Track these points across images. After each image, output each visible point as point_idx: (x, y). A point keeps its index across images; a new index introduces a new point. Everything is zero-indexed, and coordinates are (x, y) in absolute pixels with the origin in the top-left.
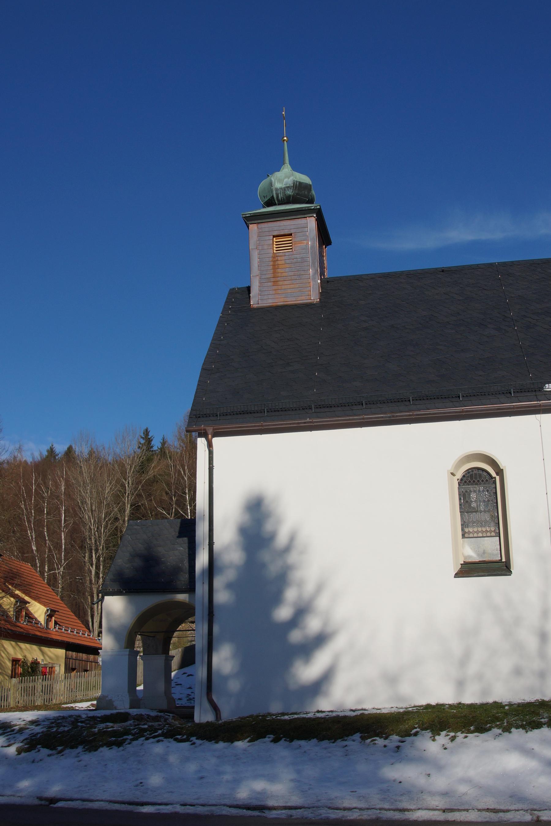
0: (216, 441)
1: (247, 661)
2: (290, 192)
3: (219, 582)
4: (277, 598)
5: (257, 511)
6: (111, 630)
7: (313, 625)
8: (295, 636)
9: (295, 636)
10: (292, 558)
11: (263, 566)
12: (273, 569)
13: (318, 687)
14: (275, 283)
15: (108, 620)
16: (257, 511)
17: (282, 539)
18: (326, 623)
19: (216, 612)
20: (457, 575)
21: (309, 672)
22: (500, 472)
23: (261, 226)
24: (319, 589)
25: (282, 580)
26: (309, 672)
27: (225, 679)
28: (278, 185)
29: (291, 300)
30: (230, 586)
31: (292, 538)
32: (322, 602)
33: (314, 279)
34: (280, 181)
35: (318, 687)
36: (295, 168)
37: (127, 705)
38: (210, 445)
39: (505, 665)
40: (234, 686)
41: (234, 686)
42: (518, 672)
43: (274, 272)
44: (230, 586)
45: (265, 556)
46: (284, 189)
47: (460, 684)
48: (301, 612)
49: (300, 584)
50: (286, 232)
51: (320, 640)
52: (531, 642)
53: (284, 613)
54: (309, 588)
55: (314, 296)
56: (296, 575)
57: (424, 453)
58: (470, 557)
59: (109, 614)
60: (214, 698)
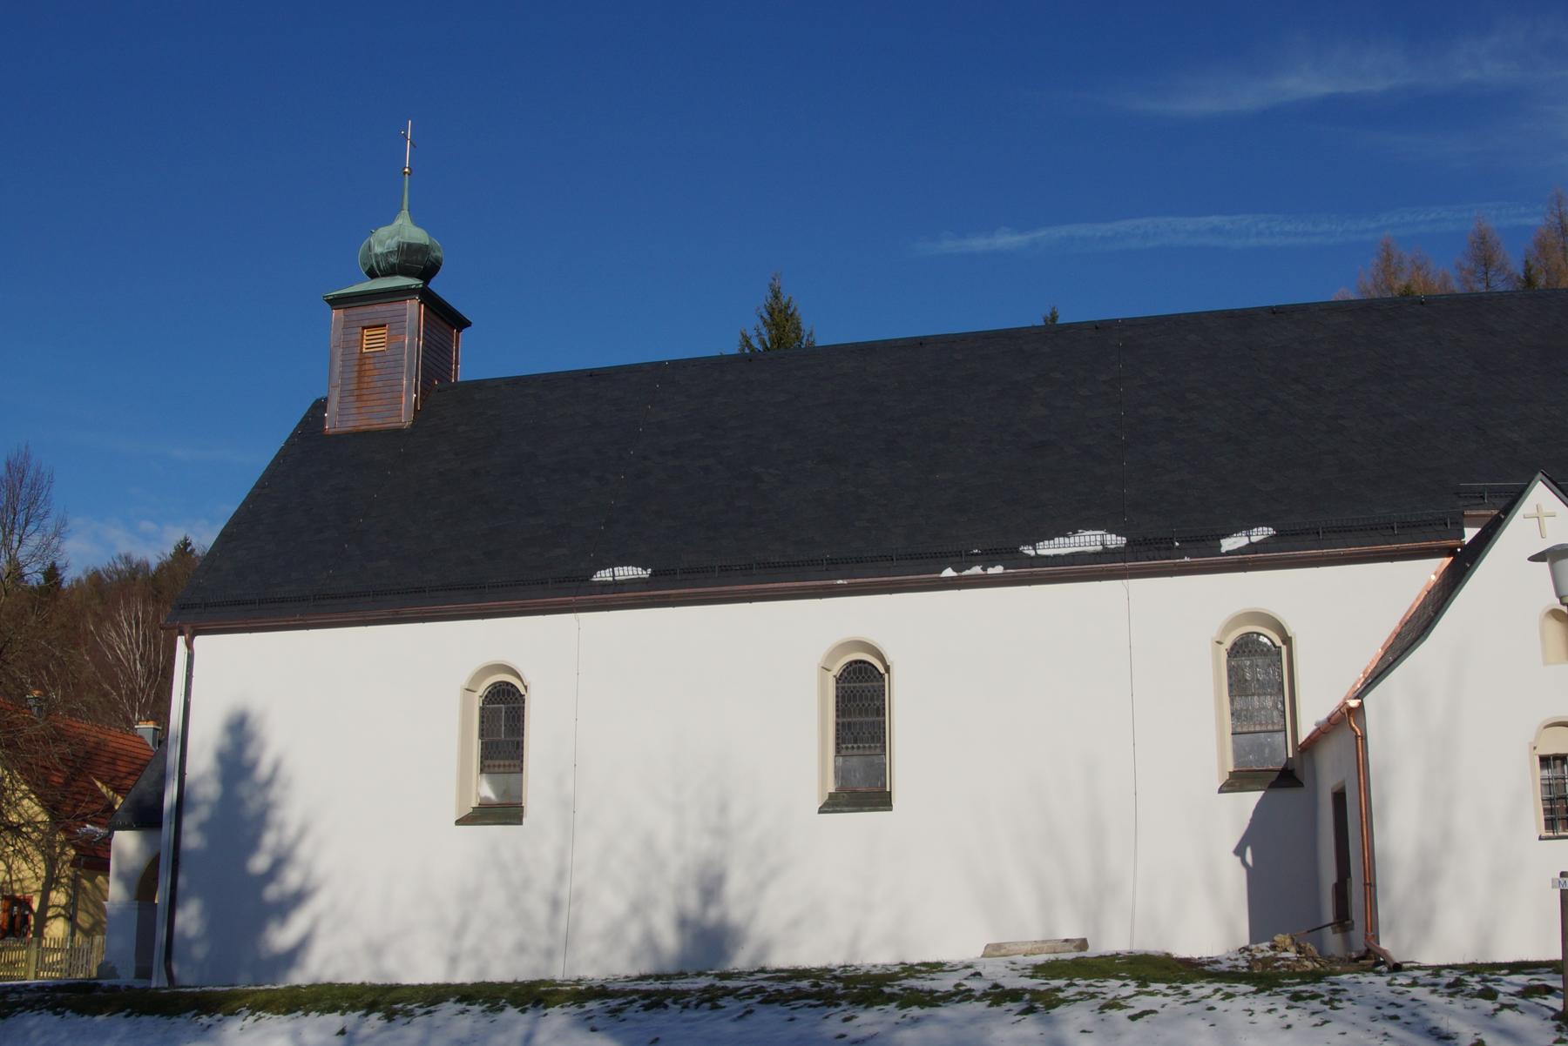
0: (200, 641)
1: (214, 920)
2: (393, 260)
3: (189, 822)
4: (253, 845)
5: (240, 730)
6: (121, 876)
7: (292, 878)
8: (272, 892)
9: (272, 892)
10: (275, 793)
12: (253, 806)
13: (292, 957)
14: (359, 398)
15: (118, 862)
16: (240, 730)
17: (264, 769)
20: (1221, 791)
21: (283, 937)
22: (887, 669)
23: (350, 311)
24: (302, 833)
26: (283, 937)
27: (189, 943)
28: (378, 250)
29: (376, 423)
30: (203, 827)
31: (276, 768)
32: (304, 851)
33: (408, 391)
34: (381, 243)
36: (417, 221)
37: (132, 974)
38: (189, 645)
39: (507, 938)
40: (199, 952)
41: (199, 952)
42: (521, 948)
43: (359, 382)
44: (203, 827)
45: (244, 790)
47: (453, 960)
48: (280, 862)
49: (281, 827)
50: (380, 322)
51: (298, 898)
52: (541, 911)
54: (291, 831)
55: (405, 418)
56: (277, 815)
57: (438, 659)
58: (487, 798)
59: (120, 855)
60: (175, 969)
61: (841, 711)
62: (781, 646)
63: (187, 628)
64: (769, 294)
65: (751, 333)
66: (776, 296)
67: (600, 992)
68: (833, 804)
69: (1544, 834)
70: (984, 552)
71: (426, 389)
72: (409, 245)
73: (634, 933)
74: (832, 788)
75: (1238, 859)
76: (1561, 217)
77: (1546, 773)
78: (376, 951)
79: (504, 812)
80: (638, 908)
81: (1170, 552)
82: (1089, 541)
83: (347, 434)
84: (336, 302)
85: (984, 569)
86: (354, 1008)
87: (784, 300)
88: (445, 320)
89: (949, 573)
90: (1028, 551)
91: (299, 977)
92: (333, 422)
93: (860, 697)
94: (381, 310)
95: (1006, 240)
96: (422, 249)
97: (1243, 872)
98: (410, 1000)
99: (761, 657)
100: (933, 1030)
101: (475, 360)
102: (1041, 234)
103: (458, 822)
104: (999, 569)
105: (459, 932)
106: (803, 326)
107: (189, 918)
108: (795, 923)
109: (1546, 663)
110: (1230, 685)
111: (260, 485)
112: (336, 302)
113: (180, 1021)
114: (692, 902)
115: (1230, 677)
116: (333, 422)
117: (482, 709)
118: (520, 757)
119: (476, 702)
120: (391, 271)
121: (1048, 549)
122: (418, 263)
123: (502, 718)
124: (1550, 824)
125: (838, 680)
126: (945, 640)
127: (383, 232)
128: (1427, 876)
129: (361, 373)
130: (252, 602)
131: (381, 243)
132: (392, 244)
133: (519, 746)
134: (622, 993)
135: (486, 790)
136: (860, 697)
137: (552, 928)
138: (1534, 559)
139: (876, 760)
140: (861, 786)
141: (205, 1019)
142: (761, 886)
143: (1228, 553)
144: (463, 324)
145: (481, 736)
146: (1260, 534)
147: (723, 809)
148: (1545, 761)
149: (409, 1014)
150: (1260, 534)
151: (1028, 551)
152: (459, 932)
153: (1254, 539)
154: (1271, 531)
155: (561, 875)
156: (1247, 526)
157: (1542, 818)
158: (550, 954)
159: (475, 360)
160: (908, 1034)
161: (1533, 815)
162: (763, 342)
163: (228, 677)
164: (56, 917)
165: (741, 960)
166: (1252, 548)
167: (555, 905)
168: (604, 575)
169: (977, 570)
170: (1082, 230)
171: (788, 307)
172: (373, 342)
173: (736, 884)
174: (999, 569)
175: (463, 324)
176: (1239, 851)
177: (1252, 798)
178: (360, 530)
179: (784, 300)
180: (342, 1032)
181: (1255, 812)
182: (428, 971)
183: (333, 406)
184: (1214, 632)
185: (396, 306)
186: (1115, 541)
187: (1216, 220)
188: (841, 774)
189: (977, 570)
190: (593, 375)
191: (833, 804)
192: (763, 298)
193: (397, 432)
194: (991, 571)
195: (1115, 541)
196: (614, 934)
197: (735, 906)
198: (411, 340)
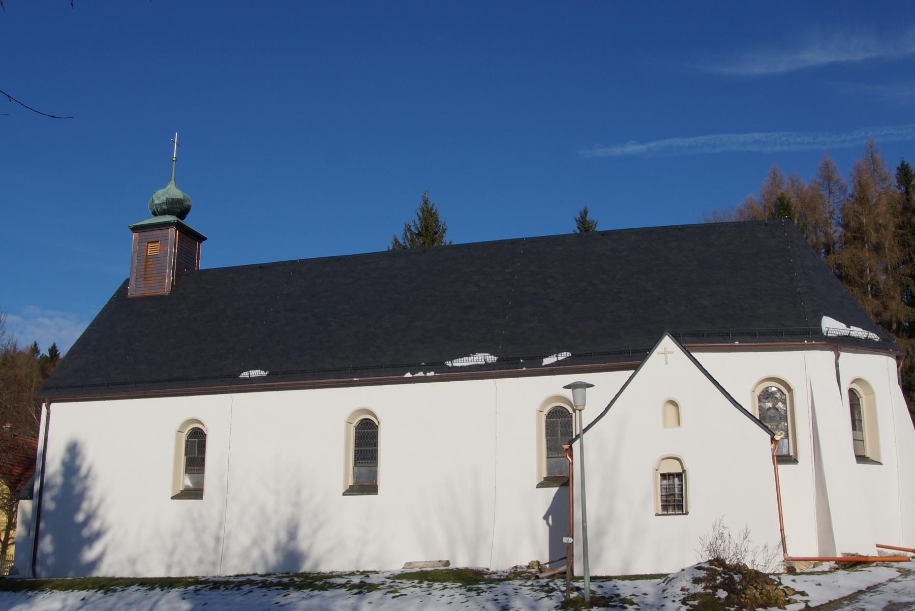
0: (53, 406)
2: (164, 207)
3: (47, 496)
4: (77, 508)
5: (73, 450)
7: (96, 525)
8: (86, 532)
9: (86, 532)
10: (89, 482)
11: (73, 487)
12: (78, 489)
13: (94, 564)
16: (73, 450)
17: (83, 471)
19: (42, 515)
21: (90, 555)
24: (101, 502)
25: (81, 496)
27: (46, 556)
28: (157, 202)
29: (153, 292)
30: (54, 499)
31: (89, 471)
32: (101, 511)
34: (158, 198)
35: (94, 564)
36: (177, 185)
38: (48, 408)
39: (195, 556)
40: (50, 561)
41: (50, 561)
42: (201, 561)
44: (54, 499)
45: (74, 480)
46: (160, 205)
47: (169, 567)
48: (89, 518)
49: (91, 500)
51: (98, 535)
52: (211, 543)
53: (80, 517)
54: (95, 502)
55: (167, 290)
56: (90, 493)
57: (158, 418)
59: (24, 512)
61: (357, 444)
62: (328, 410)
63: (46, 399)
65: (412, 224)
66: (426, 202)
67: (196, 581)
68: (350, 491)
69: (660, 512)
70: (427, 365)
72: (173, 199)
73: (255, 554)
74: (351, 483)
75: (545, 522)
76: (872, 154)
77: (665, 482)
78: (133, 562)
79: (195, 493)
80: (255, 543)
81: (518, 365)
82: (479, 359)
83: (138, 298)
84: (135, 229)
86: (93, 588)
87: (430, 206)
88: (191, 239)
89: (408, 375)
90: (449, 364)
92: (132, 292)
93: (366, 437)
95: (633, 148)
96: (179, 201)
97: (547, 528)
98: (118, 585)
100: (315, 601)
101: (209, 258)
102: (653, 145)
103: (172, 498)
105: (172, 553)
106: (440, 219)
107: (47, 545)
109: (665, 425)
110: (547, 433)
112: (135, 229)
113: (19, 594)
114: (283, 536)
115: (547, 429)
116: (132, 292)
117: (187, 441)
118: (204, 465)
119: (184, 438)
120: (164, 213)
121: (458, 363)
122: (179, 209)
123: (195, 445)
124: (665, 507)
126: (406, 408)
127: (160, 192)
128: (600, 534)
129: (146, 266)
130: (78, 387)
131: (158, 198)
132: (163, 199)
133: (203, 459)
134: (201, 583)
135: (188, 482)
136: (366, 437)
137: (216, 551)
138: (565, 387)
139: (373, 469)
140: (365, 484)
141: (30, 593)
142: (315, 532)
143: (546, 366)
144: (202, 239)
145: (186, 454)
146: (563, 356)
147: (298, 492)
148: (664, 476)
149: (115, 591)
150: (563, 356)
151: (449, 364)
152: (172, 553)
153: (560, 359)
154: (568, 354)
155: (221, 525)
156: (557, 352)
157: (660, 504)
158: (214, 564)
159: (209, 258)
160: (305, 603)
161: (655, 504)
162: (417, 228)
163: (67, 424)
164: (13, 544)
165: (306, 567)
166: (558, 363)
167: (218, 540)
168: (245, 375)
169: (421, 374)
170: (678, 142)
171: (432, 209)
172: (153, 250)
173: (303, 532)
175: (202, 239)
176: (546, 518)
177: (554, 490)
178: (137, 351)
179: (430, 206)
180: (83, 599)
181: (554, 498)
182: (158, 571)
183: (132, 283)
184: (537, 405)
185: (164, 232)
186: (491, 359)
187: (756, 136)
188: (356, 476)
189: (421, 374)
190: (262, 267)
191: (350, 491)
192: (418, 204)
193: (162, 297)
194: (428, 374)
195: (491, 359)
196: (245, 554)
197: (303, 544)
198: (171, 249)
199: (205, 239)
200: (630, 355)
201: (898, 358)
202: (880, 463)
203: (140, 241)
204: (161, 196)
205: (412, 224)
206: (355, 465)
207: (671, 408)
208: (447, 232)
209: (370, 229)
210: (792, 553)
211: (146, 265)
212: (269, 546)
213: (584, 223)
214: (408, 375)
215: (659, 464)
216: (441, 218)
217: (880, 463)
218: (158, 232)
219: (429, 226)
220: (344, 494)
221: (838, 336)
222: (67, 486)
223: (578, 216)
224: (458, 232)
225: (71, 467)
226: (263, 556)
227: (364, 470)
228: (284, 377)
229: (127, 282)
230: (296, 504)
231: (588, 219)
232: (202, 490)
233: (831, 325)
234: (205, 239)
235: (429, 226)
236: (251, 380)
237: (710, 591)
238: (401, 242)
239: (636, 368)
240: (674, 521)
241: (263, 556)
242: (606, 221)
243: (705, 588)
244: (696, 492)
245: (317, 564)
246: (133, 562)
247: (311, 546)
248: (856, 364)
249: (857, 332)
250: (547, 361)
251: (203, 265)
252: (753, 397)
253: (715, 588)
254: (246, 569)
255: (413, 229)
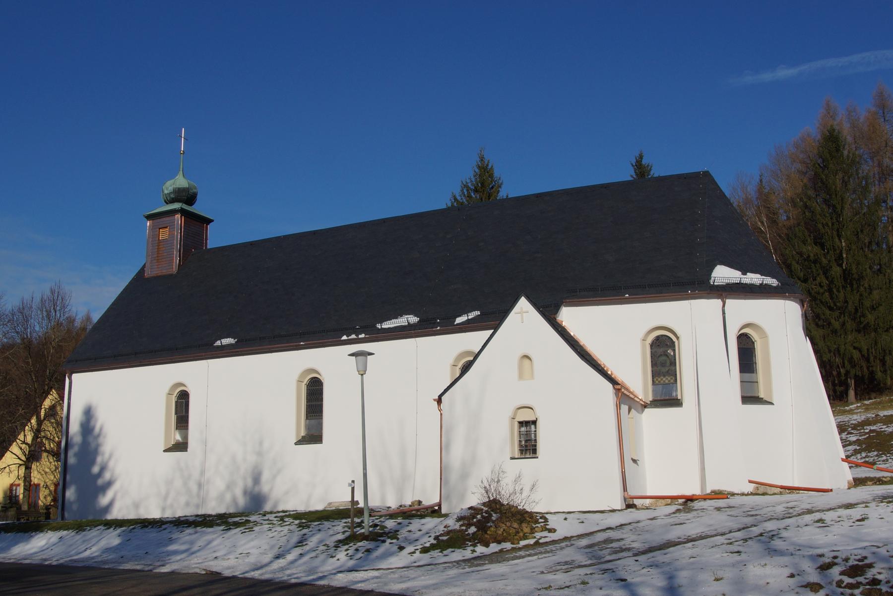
0: (74, 376)
2: (172, 196)
3: (71, 453)
4: (93, 462)
5: (88, 413)
7: (107, 476)
8: (100, 482)
10: (101, 440)
12: (93, 445)
13: (108, 508)
16: (88, 413)
17: (97, 430)
18: (112, 476)
21: (104, 501)
22: (678, 338)
28: (166, 192)
29: (165, 272)
30: (76, 455)
31: (101, 429)
32: (111, 464)
34: (167, 189)
39: (183, 500)
40: (75, 507)
41: (75, 507)
42: (187, 504)
44: (76, 455)
45: (90, 439)
47: (163, 510)
48: (103, 469)
49: (103, 454)
51: (109, 484)
52: (194, 488)
54: (107, 456)
61: (654, 364)
64: (478, 159)
65: (468, 181)
68: (301, 441)
70: (361, 327)
71: (185, 253)
72: (179, 189)
73: (228, 497)
74: (303, 433)
78: (136, 506)
79: (181, 447)
80: (229, 487)
81: (435, 324)
84: (149, 217)
85: (357, 335)
88: (197, 223)
89: (345, 338)
90: (379, 326)
91: (110, 517)
92: (148, 274)
94: (166, 219)
95: (784, 73)
99: (274, 375)
101: (216, 238)
103: (296, 444)
104: (363, 336)
107: (70, 494)
108: (287, 493)
111: (113, 304)
112: (149, 217)
114: (250, 482)
116: (148, 274)
117: (176, 402)
119: (174, 399)
120: (172, 201)
121: (387, 325)
122: (187, 197)
125: (652, 346)
127: (169, 183)
132: (171, 189)
135: (178, 437)
137: (198, 495)
142: (274, 477)
143: (458, 324)
144: (209, 221)
145: (176, 413)
147: (261, 443)
148: (521, 423)
150: (472, 315)
151: (379, 326)
154: (478, 313)
155: (202, 473)
158: (197, 506)
159: (216, 238)
163: (88, 390)
167: (200, 486)
168: (218, 343)
169: (353, 336)
172: (164, 234)
173: (266, 476)
174: (363, 336)
175: (209, 221)
186: (413, 319)
188: (308, 428)
189: (353, 336)
192: (475, 161)
193: (171, 275)
194: (360, 336)
195: (413, 319)
196: (221, 498)
197: (265, 488)
199: (212, 221)
200: (493, 318)
201: (802, 303)
202: (772, 404)
203: (153, 228)
204: (169, 187)
205: (468, 181)
206: (307, 418)
207: (527, 361)
208: (503, 186)
209: (433, 190)
210: (632, 492)
211: (158, 248)
212: (238, 492)
213: (641, 169)
214: (345, 338)
215: (515, 414)
216: (496, 174)
217: (772, 404)
218: (167, 219)
219: (485, 182)
220: (296, 444)
221: (728, 284)
222: (85, 444)
223: (634, 161)
224: (513, 186)
225: (87, 427)
226: (234, 501)
227: (313, 422)
228: (249, 344)
229: (144, 266)
230: (260, 454)
231: (643, 162)
232: (187, 443)
233: (723, 274)
234: (212, 221)
235: (485, 182)
236: (222, 347)
237: (464, 528)
238: (459, 198)
239: (496, 328)
240: (527, 464)
241: (234, 501)
242: (662, 167)
243: (461, 526)
244: (544, 437)
245: (276, 504)
246: (136, 506)
247: (271, 489)
248: (743, 311)
249: (753, 278)
250: (459, 320)
251: (211, 244)
252: (643, 347)
253: (469, 525)
254: (222, 510)
255: (470, 185)
